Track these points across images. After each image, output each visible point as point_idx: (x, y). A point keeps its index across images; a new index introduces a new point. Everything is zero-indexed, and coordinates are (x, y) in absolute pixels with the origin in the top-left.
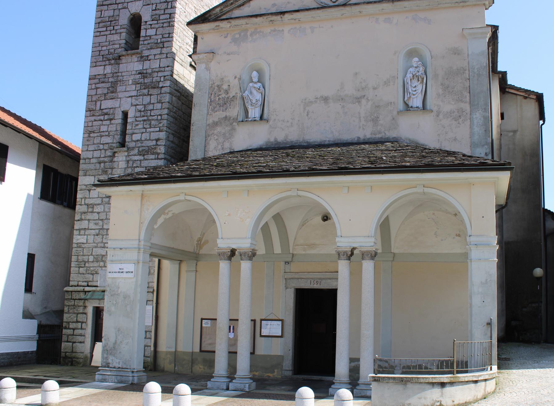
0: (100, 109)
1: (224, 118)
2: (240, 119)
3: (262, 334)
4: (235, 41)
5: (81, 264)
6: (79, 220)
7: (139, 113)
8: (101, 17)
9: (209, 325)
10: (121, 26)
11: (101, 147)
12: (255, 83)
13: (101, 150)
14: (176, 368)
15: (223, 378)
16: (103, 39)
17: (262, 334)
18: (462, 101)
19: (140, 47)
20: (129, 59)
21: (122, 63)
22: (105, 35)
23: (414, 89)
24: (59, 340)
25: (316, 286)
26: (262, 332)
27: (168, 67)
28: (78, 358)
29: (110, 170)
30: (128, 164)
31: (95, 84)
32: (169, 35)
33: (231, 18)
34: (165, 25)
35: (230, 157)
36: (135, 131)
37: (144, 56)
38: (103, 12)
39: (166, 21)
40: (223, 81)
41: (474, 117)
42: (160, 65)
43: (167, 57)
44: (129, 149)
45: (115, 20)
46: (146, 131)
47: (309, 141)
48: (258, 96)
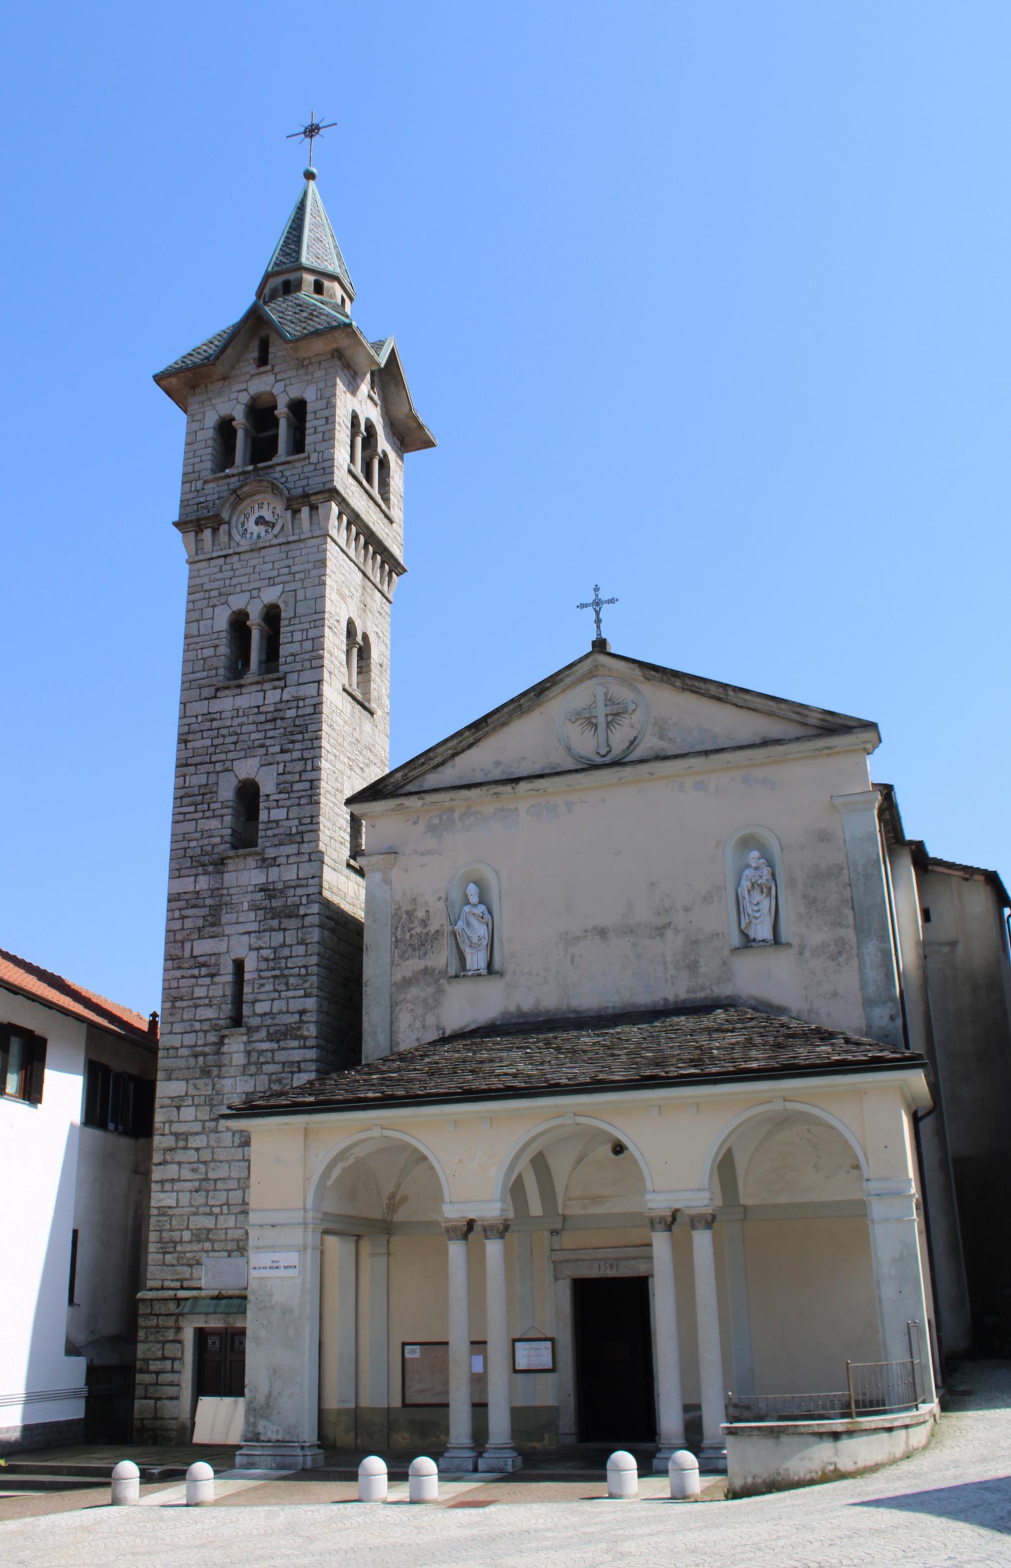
0: (192, 956)
1: (422, 970)
2: (452, 972)
3: (517, 1368)
4: (432, 829)
5: (168, 1248)
6: (160, 1164)
7: (265, 963)
8: (184, 787)
9: (417, 1355)
10: (222, 802)
11: (197, 1026)
12: (474, 905)
13: (196, 1032)
14: (359, 1441)
15: (466, 1451)
16: (189, 826)
17: (517, 1368)
18: (841, 925)
19: (260, 841)
20: (241, 863)
21: (227, 872)
22: (193, 820)
23: (756, 908)
24: (128, 1392)
25: (610, 1273)
26: (517, 1364)
27: (313, 877)
28: (166, 1430)
29: (215, 1069)
30: (249, 1058)
31: (180, 910)
32: (312, 820)
33: (425, 792)
34: (303, 801)
35: (447, 1052)
36: (260, 997)
37: (268, 858)
38: (188, 778)
39: (303, 793)
40: (416, 904)
41: (865, 951)
42: (298, 875)
43: (310, 860)
44: (251, 1030)
45: (211, 793)
46: (280, 996)
47: (578, 1009)
48: (481, 930)
